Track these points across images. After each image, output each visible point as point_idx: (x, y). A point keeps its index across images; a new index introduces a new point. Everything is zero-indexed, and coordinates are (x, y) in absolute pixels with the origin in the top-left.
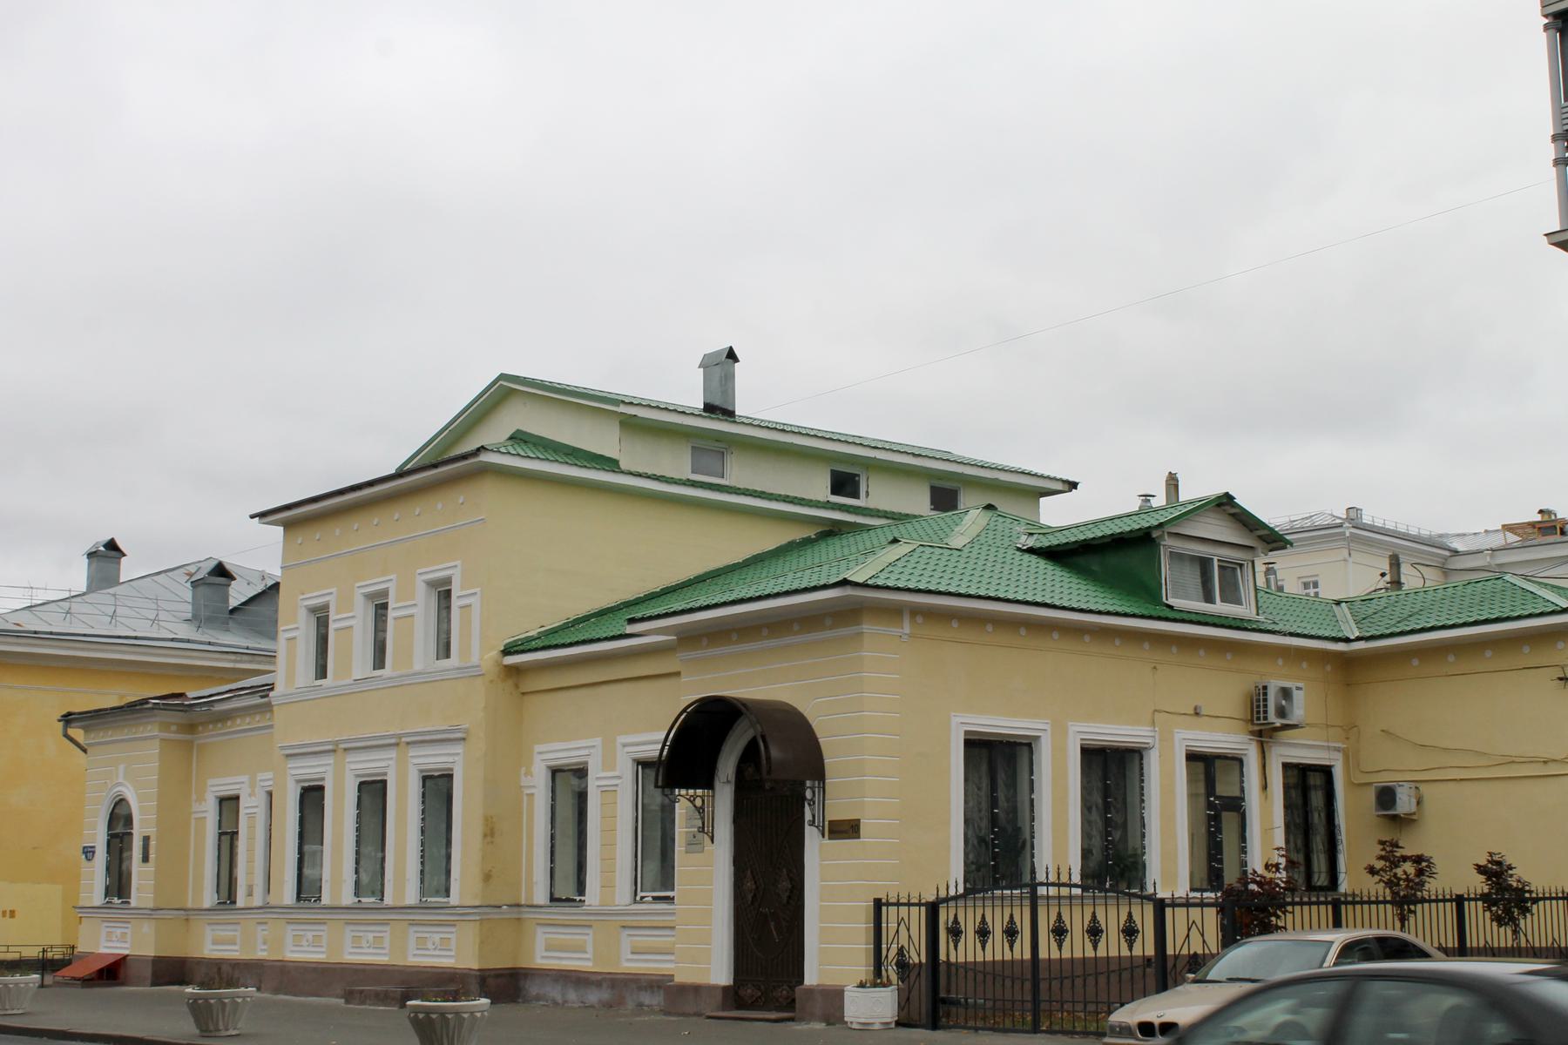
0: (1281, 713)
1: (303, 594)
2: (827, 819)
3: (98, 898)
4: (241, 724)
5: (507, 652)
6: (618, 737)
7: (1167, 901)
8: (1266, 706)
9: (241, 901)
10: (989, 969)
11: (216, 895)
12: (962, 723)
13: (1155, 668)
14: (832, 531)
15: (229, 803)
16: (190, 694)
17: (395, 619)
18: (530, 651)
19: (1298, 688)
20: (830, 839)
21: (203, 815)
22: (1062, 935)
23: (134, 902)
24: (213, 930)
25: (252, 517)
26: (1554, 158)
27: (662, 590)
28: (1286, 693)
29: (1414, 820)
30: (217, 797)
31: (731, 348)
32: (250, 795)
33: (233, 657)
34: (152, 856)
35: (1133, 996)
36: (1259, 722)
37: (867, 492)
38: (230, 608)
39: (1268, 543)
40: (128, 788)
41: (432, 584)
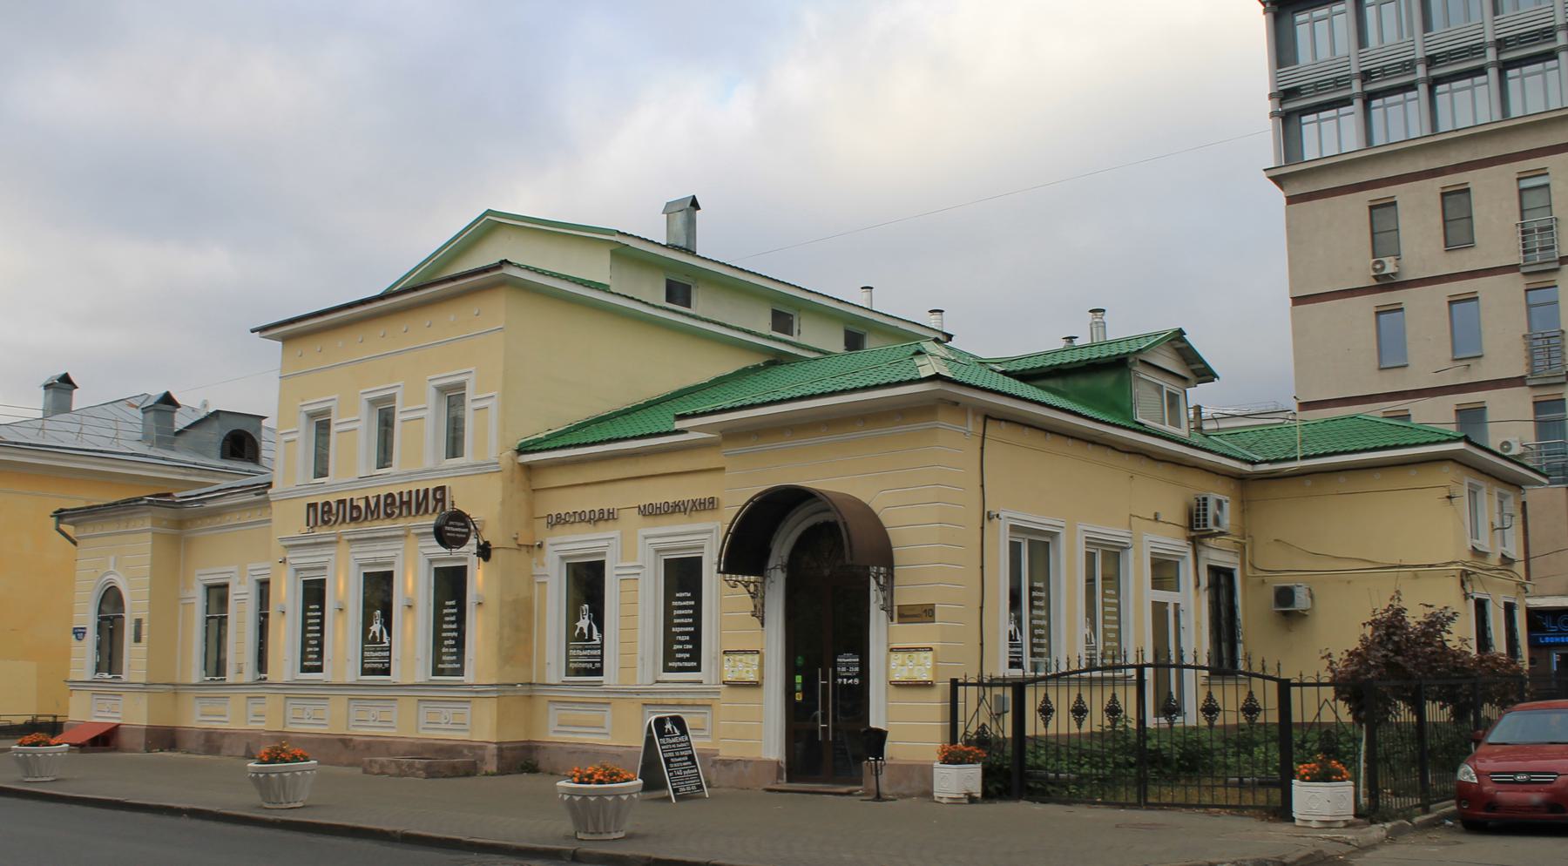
0: (1217, 522)
1: (303, 400)
2: (896, 603)
3: (87, 673)
4: (234, 519)
5: (522, 450)
6: (547, 539)
7: (960, 681)
8: (1205, 515)
9: (231, 677)
10: (1063, 742)
11: (204, 672)
12: (1009, 518)
13: (1132, 477)
14: (777, 360)
15: (218, 594)
16: (176, 495)
17: (403, 421)
18: (548, 450)
19: (1227, 501)
20: (899, 623)
21: (192, 601)
22: (1214, 713)
23: (124, 678)
25: (253, 331)
26: (1270, 111)
27: (646, 403)
28: (1220, 504)
29: (1306, 616)
30: (205, 585)
31: (694, 196)
32: (239, 583)
33: (183, 471)
34: (144, 637)
37: (799, 331)
38: (176, 430)
39: (1198, 376)
40: (115, 574)
41: (441, 390)
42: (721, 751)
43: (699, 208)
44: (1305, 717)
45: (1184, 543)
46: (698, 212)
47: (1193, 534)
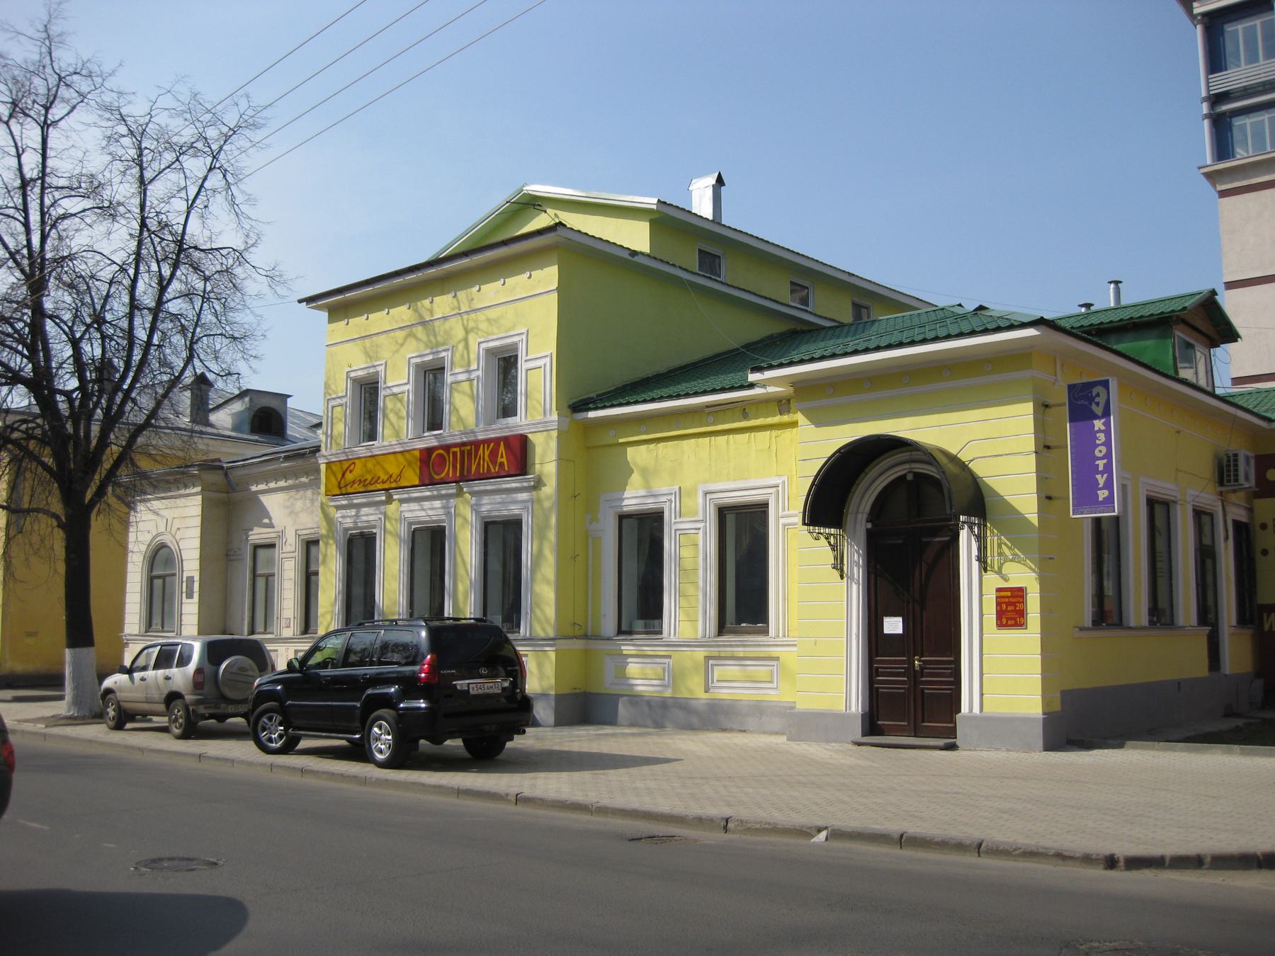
13: (1178, 432)
24: (1175, 497)
25: (300, 301)
35: (562, 459)
36: (1229, 484)
42: (797, 703)
43: (724, 185)
44: (187, 605)
45: (1214, 497)
46: (722, 188)
47: (1223, 489)
